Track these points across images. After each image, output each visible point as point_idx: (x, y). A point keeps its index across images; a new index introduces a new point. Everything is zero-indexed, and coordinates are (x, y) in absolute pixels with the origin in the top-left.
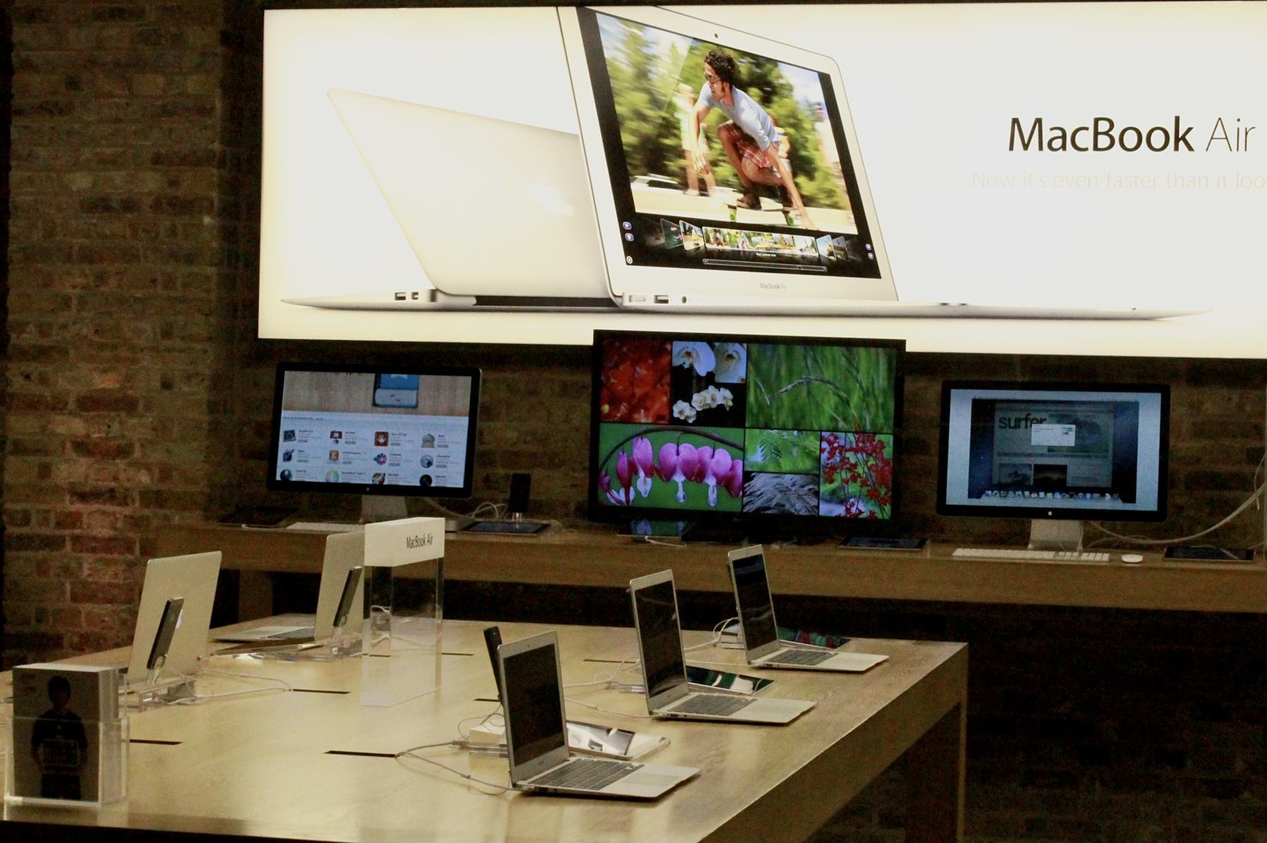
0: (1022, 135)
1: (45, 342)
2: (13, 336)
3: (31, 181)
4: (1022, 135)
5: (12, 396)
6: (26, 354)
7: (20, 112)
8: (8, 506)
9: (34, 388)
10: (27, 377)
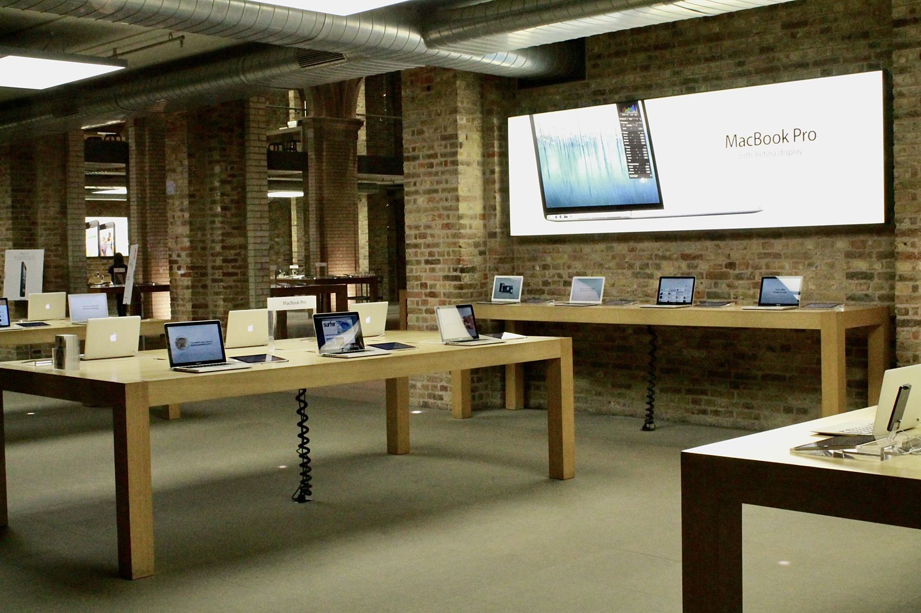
0: (731, 141)
1: (914, 227)
2: (898, 225)
3: (904, 150)
4: (731, 141)
5: (898, 253)
6: (903, 234)
7: (897, 118)
8: (898, 306)
9: (909, 249)
10: (905, 244)
